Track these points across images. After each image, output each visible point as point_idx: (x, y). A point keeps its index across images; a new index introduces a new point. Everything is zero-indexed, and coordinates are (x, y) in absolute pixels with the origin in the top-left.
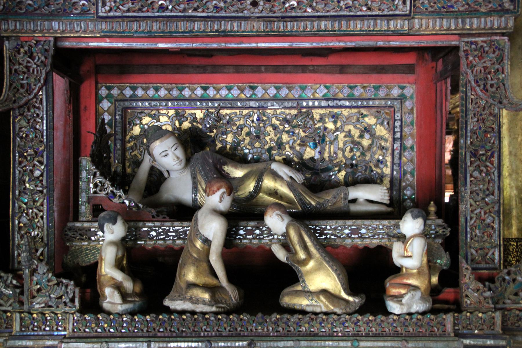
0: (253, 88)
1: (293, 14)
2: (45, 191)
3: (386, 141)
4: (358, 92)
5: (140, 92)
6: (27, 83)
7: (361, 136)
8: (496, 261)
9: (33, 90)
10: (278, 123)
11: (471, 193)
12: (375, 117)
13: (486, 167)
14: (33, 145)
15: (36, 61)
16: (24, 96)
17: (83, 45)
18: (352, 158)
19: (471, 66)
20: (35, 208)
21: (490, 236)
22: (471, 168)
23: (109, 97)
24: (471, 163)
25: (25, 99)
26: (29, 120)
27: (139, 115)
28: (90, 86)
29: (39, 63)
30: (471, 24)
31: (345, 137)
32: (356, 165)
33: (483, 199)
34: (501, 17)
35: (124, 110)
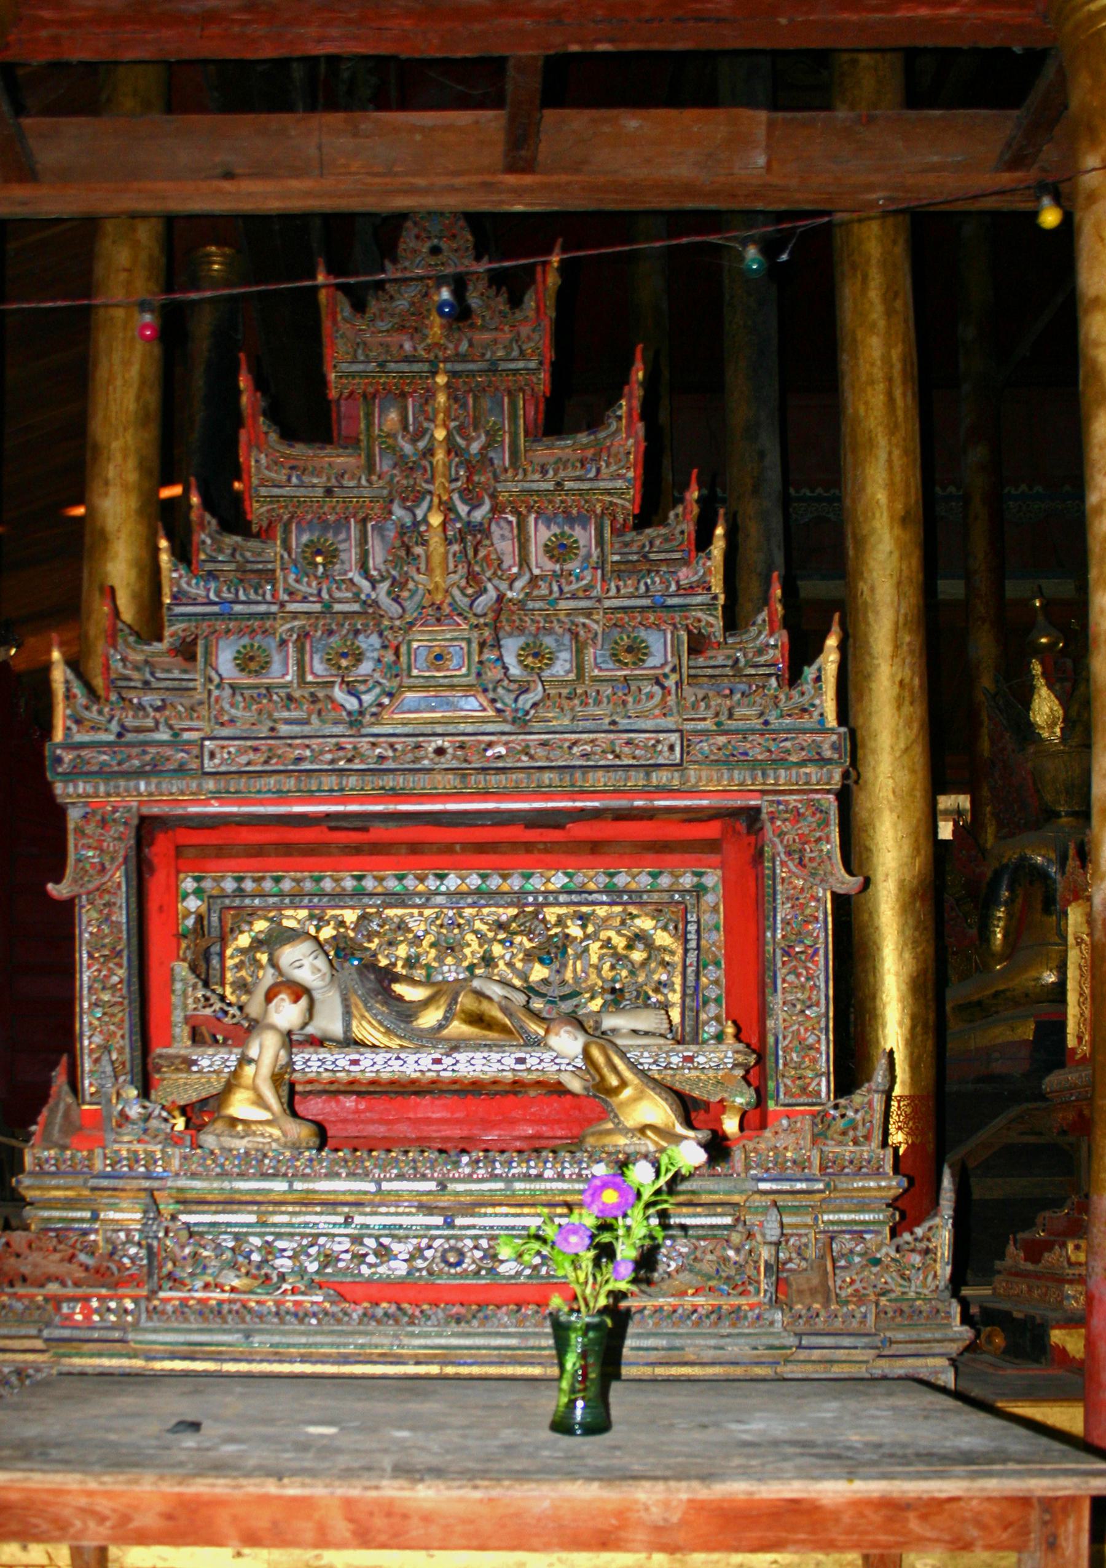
3: (672, 953)
4: (621, 880)
7: (630, 947)
8: (823, 1094)
11: (784, 1003)
12: (653, 918)
13: (807, 968)
17: (180, 811)
18: (614, 980)
19: (781, 835)
21: (814, 1061)
22: (784, 971)
23: (198, 892)
24: (784, 963)
30: (777, 778)
31: (601, 947)
32: (621, 990)
33: (802, 1012)
34: (822, 768)
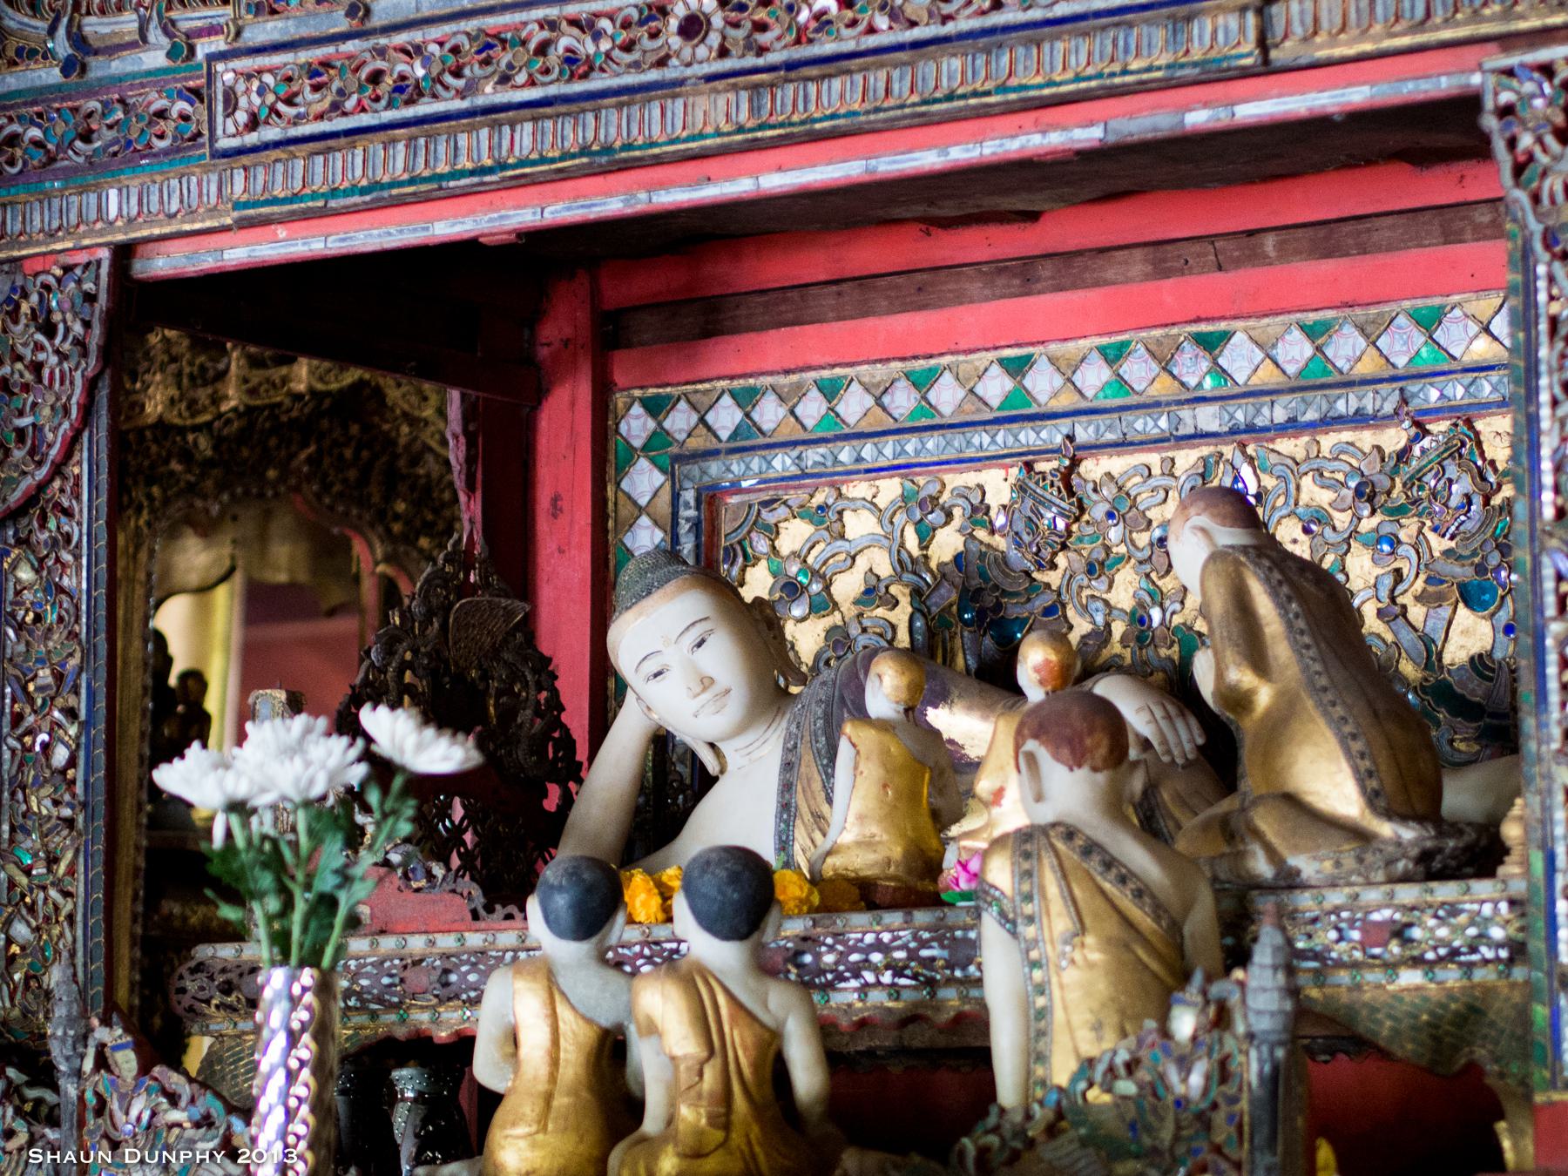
0: (1211, 344)
1: (828, 47)
2: (80, 819)
5: (769, 413)
6: (34, 425)
9: (50, 446)
10: (1325, 497)
14: (49, 652)
15: (57, 341)
16: (24, 473)
20: (53, 884)
25: (27, 483)
26: (41, 560)
27: (769, 517)
28: (573, 404)
29: (67, 346)
35: (710, 498)
